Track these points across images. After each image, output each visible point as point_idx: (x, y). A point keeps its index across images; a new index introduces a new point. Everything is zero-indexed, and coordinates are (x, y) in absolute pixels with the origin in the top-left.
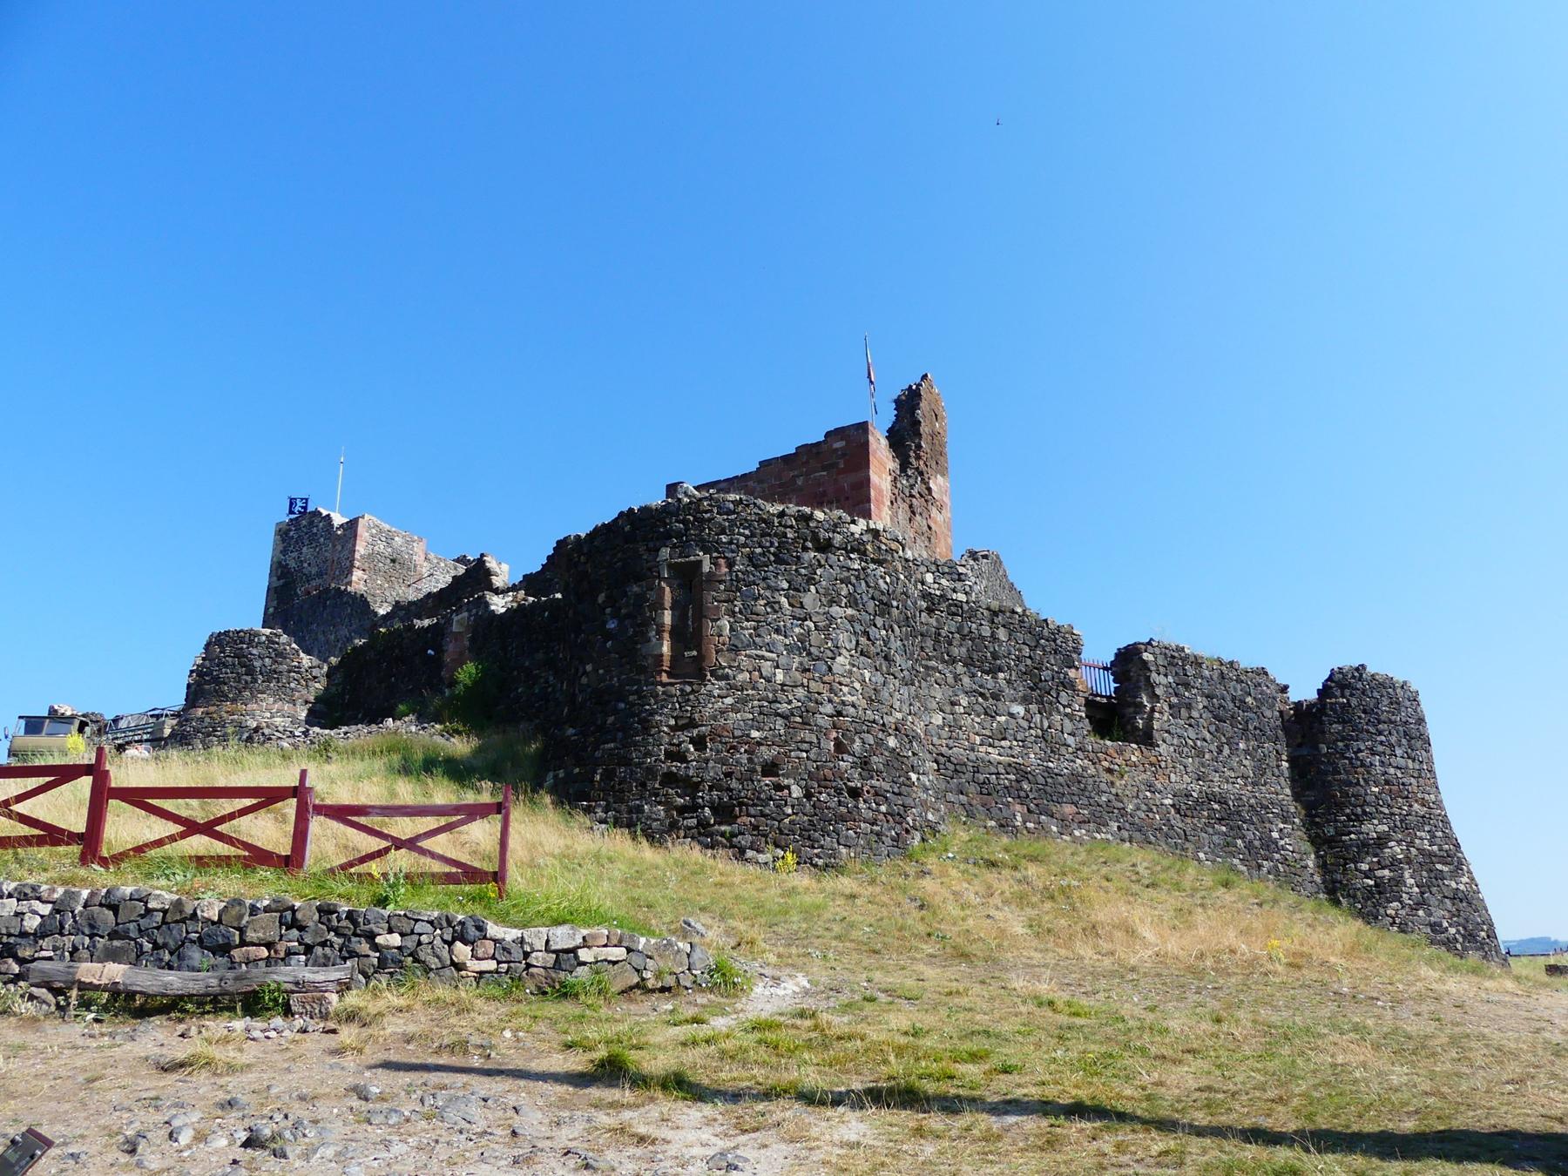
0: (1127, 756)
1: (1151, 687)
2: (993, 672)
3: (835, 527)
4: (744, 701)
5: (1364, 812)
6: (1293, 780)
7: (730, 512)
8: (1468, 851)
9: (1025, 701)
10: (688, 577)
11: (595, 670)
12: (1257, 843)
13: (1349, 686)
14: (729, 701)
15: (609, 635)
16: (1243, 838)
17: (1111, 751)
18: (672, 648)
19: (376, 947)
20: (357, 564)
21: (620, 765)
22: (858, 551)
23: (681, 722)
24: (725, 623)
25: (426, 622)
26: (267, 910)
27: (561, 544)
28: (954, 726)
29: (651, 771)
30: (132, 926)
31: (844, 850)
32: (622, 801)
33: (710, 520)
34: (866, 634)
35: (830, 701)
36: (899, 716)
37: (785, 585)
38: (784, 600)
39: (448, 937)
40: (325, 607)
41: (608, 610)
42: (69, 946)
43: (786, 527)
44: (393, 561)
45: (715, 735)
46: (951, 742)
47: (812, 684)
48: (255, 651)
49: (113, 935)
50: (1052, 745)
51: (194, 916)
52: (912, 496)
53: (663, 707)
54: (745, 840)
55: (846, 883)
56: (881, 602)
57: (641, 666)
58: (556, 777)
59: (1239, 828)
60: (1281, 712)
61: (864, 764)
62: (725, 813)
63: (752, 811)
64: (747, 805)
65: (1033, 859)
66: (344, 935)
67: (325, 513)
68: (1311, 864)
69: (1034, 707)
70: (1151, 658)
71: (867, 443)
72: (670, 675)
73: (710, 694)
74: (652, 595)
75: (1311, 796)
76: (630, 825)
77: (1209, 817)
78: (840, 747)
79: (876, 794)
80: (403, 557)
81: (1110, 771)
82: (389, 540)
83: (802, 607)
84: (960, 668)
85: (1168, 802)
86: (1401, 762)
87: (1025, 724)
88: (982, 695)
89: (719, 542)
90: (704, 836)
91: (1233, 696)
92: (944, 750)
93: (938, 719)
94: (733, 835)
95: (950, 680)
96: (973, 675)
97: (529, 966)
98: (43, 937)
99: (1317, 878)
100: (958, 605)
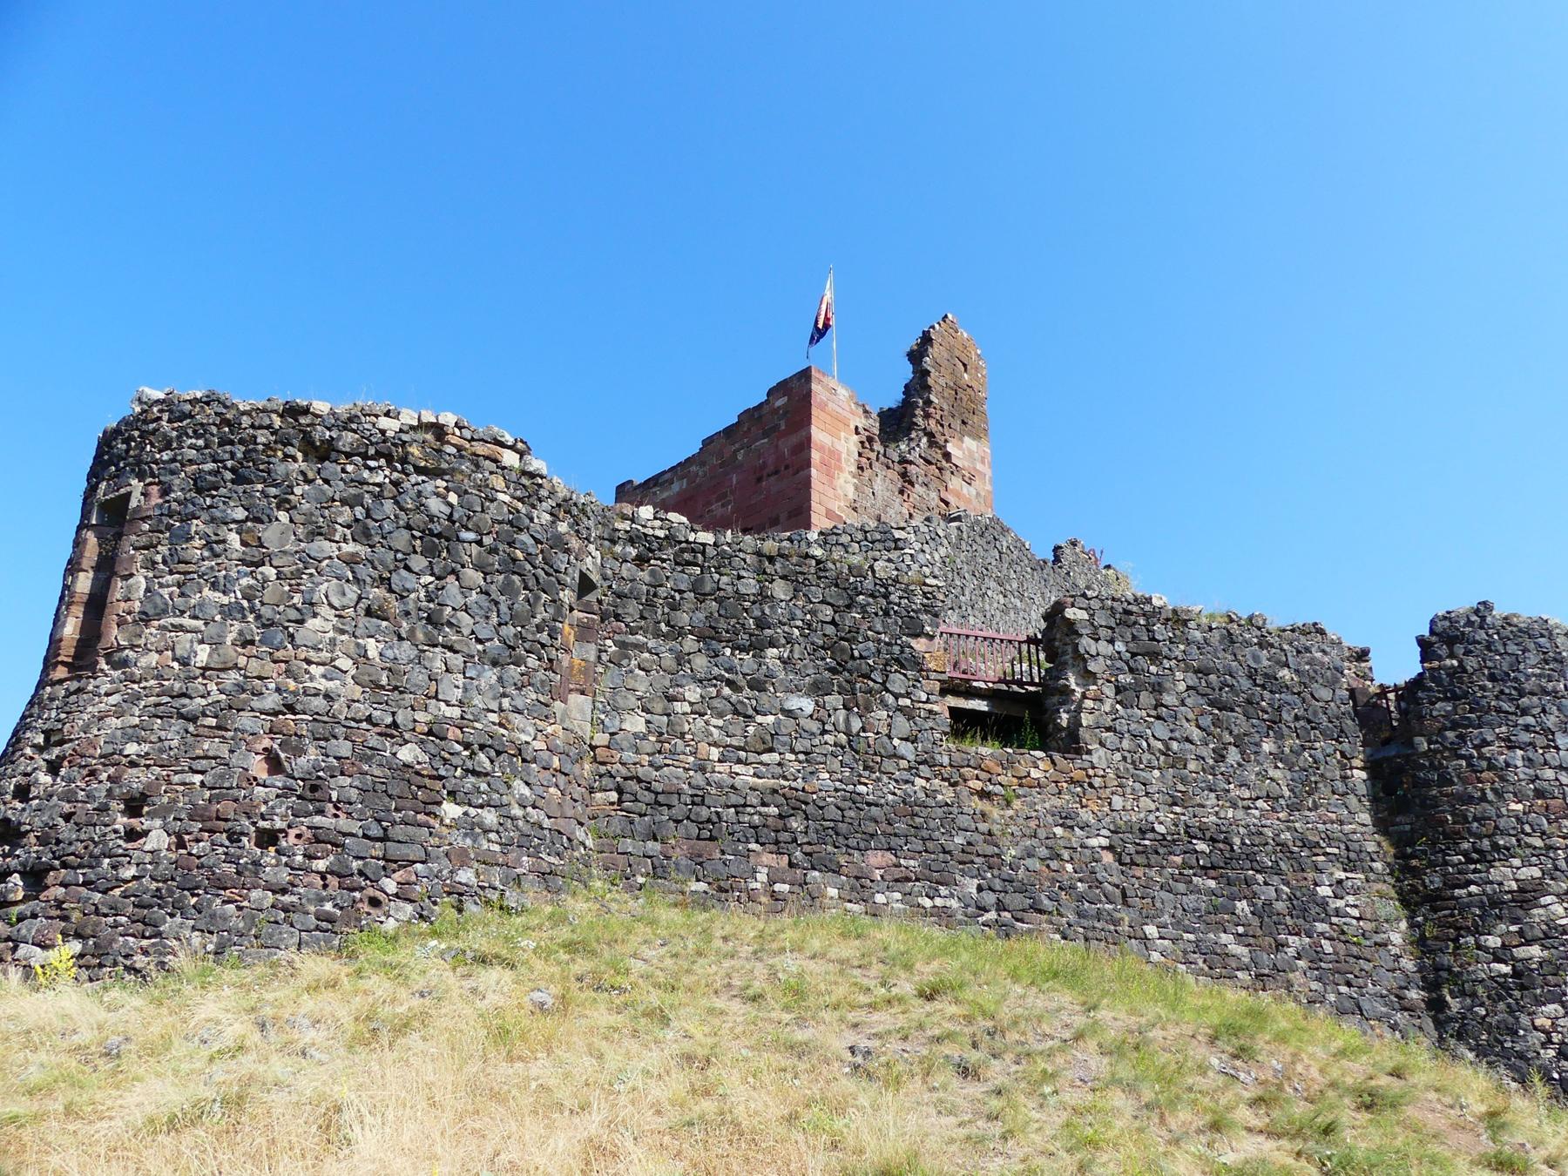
1: (1081, 659)
2: (757, 647)
5: (1496, 847)
6: (1374, 800)
9: (818, 689)
12: (1280, 906)
16: (1251, 898)
17: (988, 763)
24: (140, 582)
28: (667, 735)
34: (384, 581)
37: (240, 514)
38: (234, 539)
46: (659, 759)
50: (865, 756)
59: (1248, 882)
60: (1352, 692)
68: (1396, 938)
69: (834, 700)
70: (1083, 615)
71: (809, 394)
75: (1405, 823)
77: (1185, 865)
84: (690, 643)
87: (814, 726)
88: (730, 684)
93: (636, 723)
95: (668, 660)
99: (1408, 964)
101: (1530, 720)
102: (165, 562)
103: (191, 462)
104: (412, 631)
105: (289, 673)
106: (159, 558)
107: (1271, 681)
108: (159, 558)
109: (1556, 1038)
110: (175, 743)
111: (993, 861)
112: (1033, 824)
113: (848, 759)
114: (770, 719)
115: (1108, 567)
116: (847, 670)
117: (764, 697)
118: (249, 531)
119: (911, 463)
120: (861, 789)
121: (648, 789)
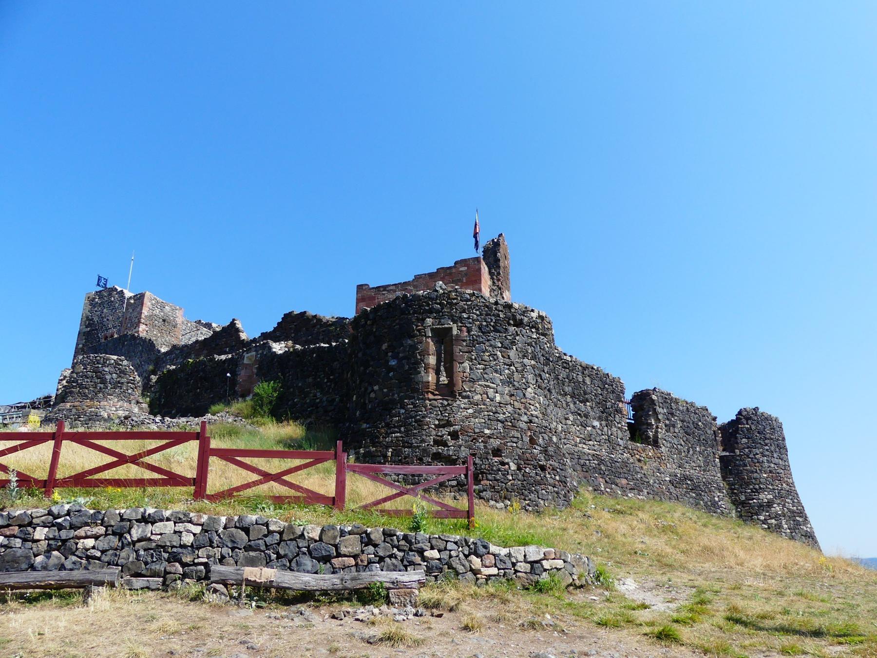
1: (656, 414)
2: (584, 402)
4: (480, 411)
5: (760, 488)
8: (807, 511)
9: (600, 419)
10: (443, 337)
11: (381, 389)
13: (750, 418)
14: (471, 411)
15: (391, 369)
19: (424, 559)
20: (142, 321)
22: (535, 327)
24: (466, 364)
25: (223, 357)
26: (350, 533)
27: (288, 317)
30: (261, 542)
33: (456, 304)
35: (526, 414)
37: (500, 345)
38: (499, 353)
39: (467, 553)
40: (123, 345)
41: (390, 354)
42: (218, 556)
43: (499, 311)
44: (164, 321)
45: (463, 430)
47: (516, 403)
48: (106, 369)
49: (248, 548)
50: (612, 444)
51: (302, 536)
54: (487, 494)
57: (416, 390)
63: (489, 477)
66: (404, 551)
67: (119, 289)
73: (459, 407)
78: (532, 441)
79: (553, 469)
80: (177, 318)
81: (639, 461)
82: (162, 307)
83: (509, 358)
84: (569, 399)
85: (668, 479)
86: (777, 461)
87: (600, 432)
88: (579, 415)
91: (693, 420)
94: (480, 491)
95: (564, 405)
97: (516, 571)
98: (198, 548)
100: (566, 362)
103: (478, 320)
107: (697, 427)
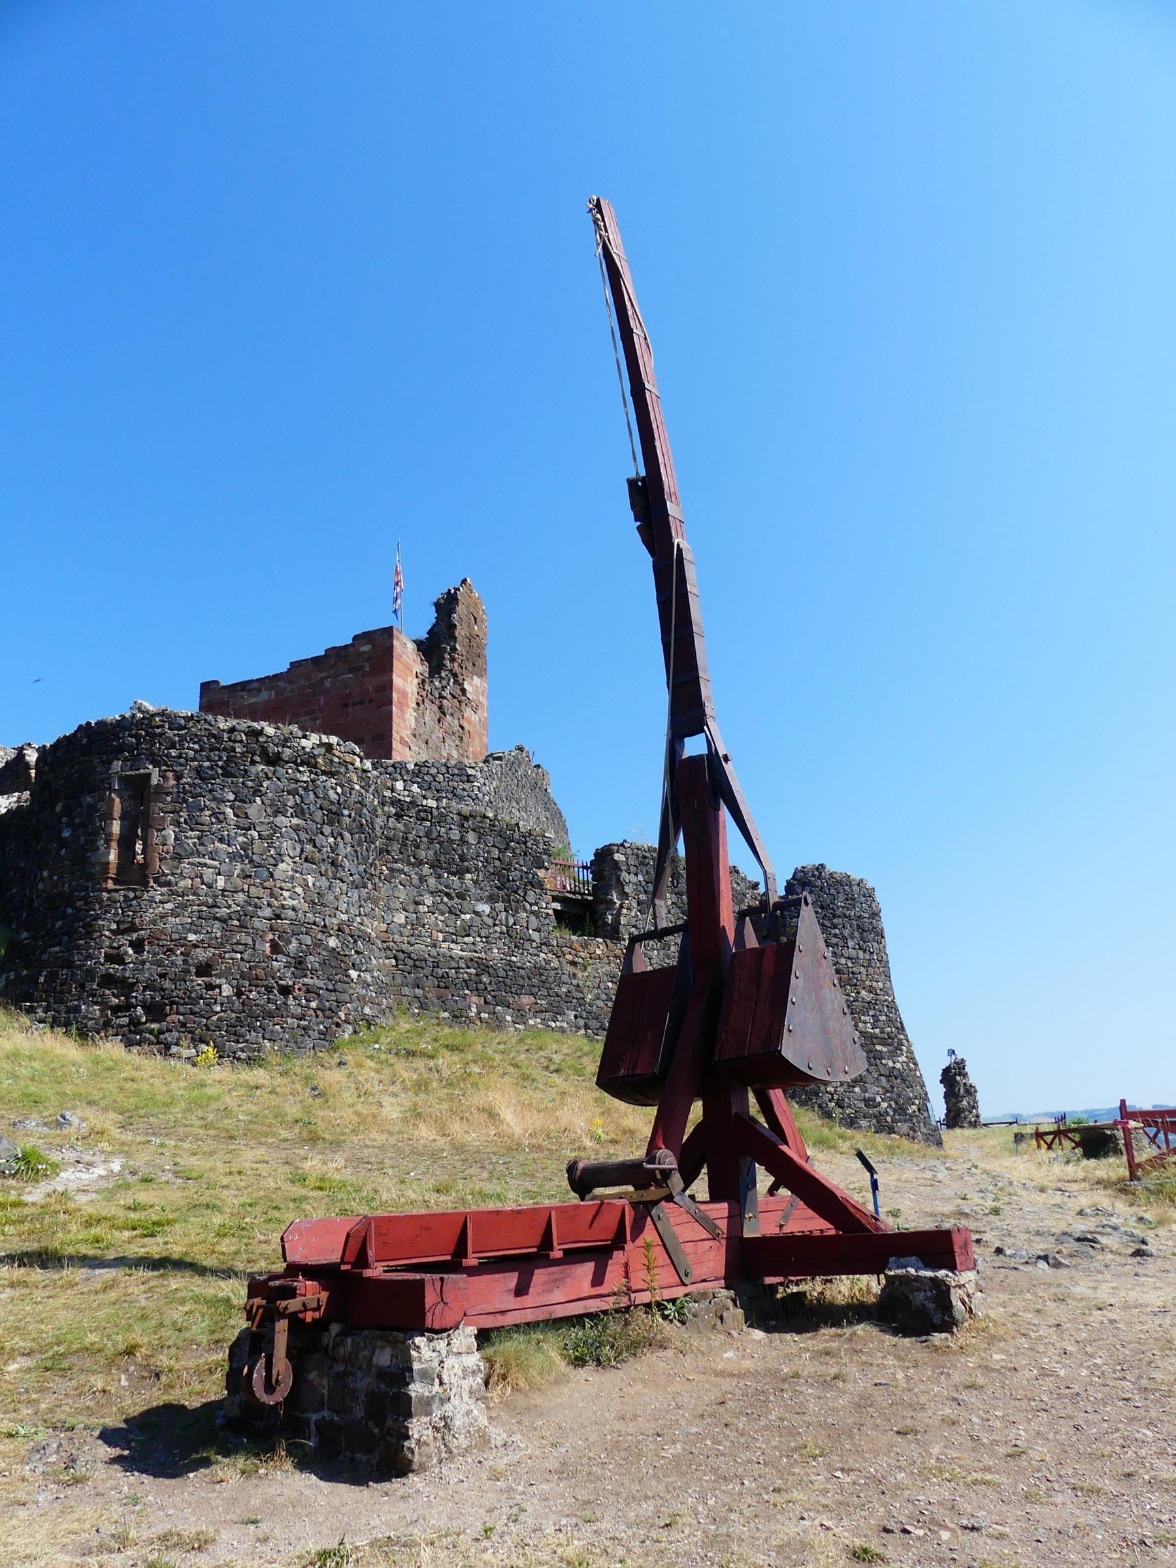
0: (592, 950)
1: (620, 885)
2: (460, 873)
3: (285, 743)
4: (184, 906)
7: (181, 728)
9: (492, 899)
11: (50, 877)
14: (169, 906)
15: (63, 843)
17: (576, 945)
18: (120, 856)
21: (62, 967)
22: (308, 764)
23: (122, 927)
24: (170, 833)
29: (90, 973)
31: (268, 1044)
32: (62, 1001)
33: (161, 735)
34: (312, 842)
35: (269, 905)
36: (345, 917)
37: (231, 797)
38: (229, 811)
41: (64, 820)
45: (153, 939)
46: (412, 940)
47: (253, 889)
50: (516, 940)
52: (441, 697)
53: (106, 912)
54: (168, 1037)
55: (258, 1075)
56: (330, 811)
57: (93, 874)
58: (8, 977)
61: (299, 964)
62: (155, 1011)
64: (177, 1004)
65: (452, 1048)
69: (500, 906)
70: (623, 858)
72: (116, 881)
73: (152, 900)
74: (102, 806)
76: (67, 1024)
78: (275, 948)
79: (308, 991)
83: (247, 817)
84: (426, 869)
86: (853, 953)
87: (490, 921)
88: (447, 895)
89: (168, 756)
90: (132, 1036)
92: (405, 947)
93: (400, 918)
94: (161, 1032)
96: (440, 877)
100: (429, 810)
101: (837, 931)
102: (186, 822)
103: (193, 759)
104: (326, 870)
105: (272, 895)
106: (182, 820)
108: (182, 820)
109: (836, 1097)
110: (219, 935)
111: (581, 1001)
112: (598, 980)
113: (507, 941)
114: (468, 916)
115: (538, 766)
116: (508, 889)
117: (465, 903)
118: (239, 807)
119: (445, 698)
120: (514, 959)
121: (409, 957)
